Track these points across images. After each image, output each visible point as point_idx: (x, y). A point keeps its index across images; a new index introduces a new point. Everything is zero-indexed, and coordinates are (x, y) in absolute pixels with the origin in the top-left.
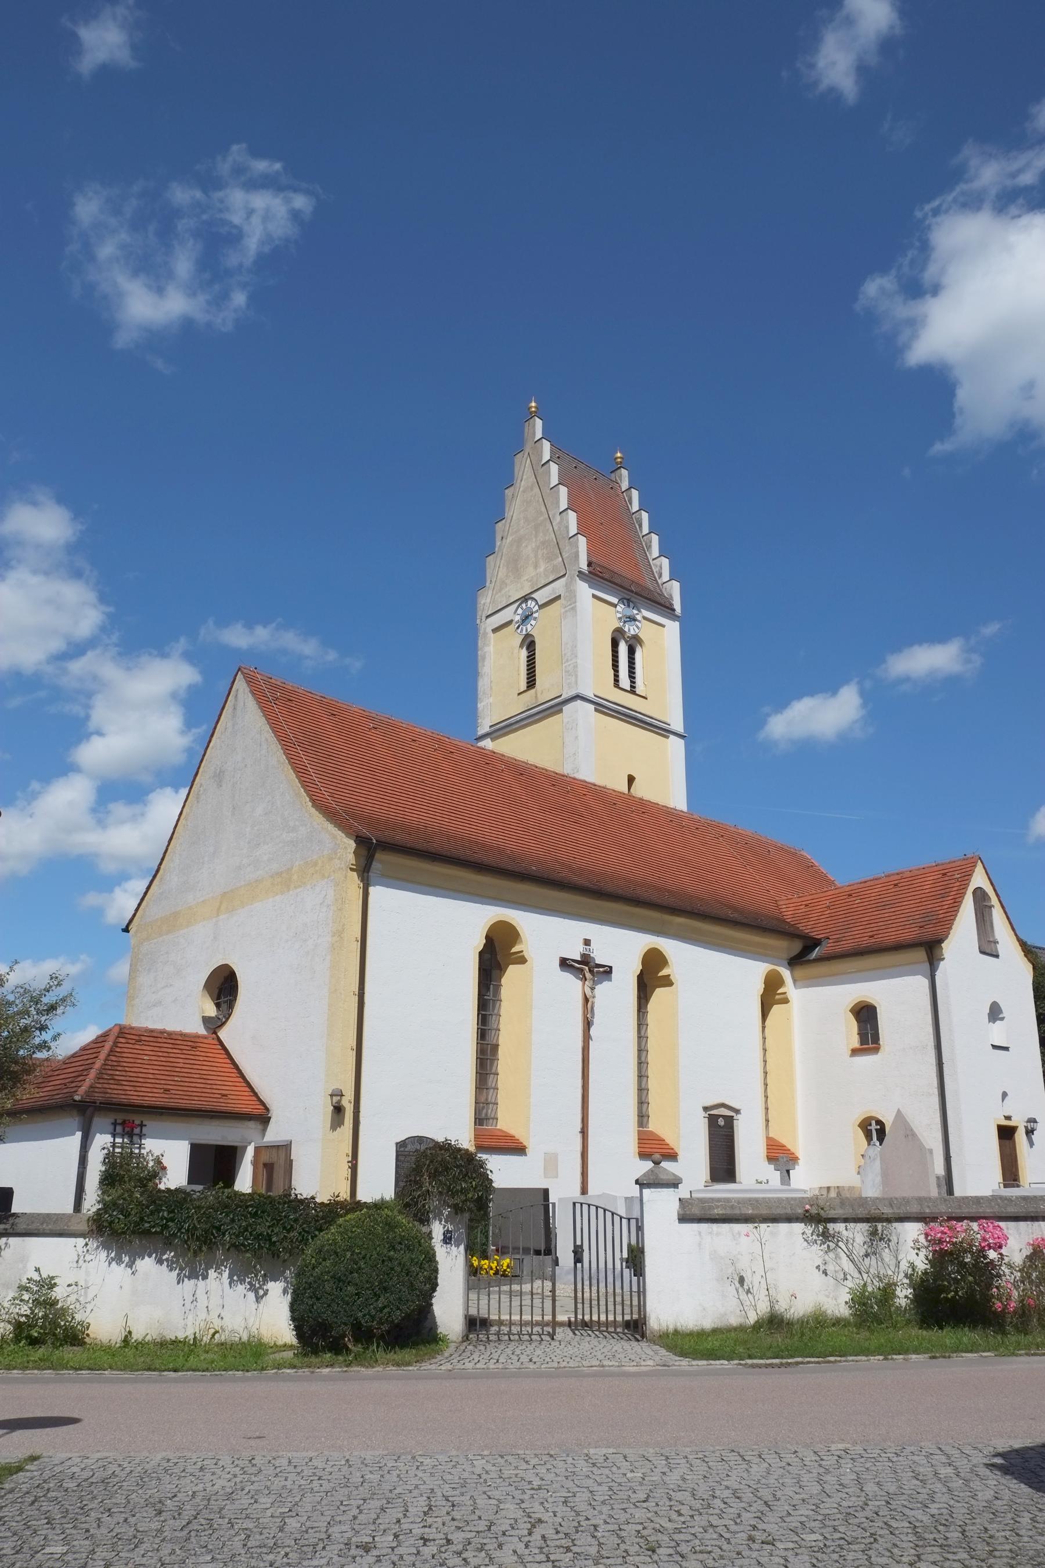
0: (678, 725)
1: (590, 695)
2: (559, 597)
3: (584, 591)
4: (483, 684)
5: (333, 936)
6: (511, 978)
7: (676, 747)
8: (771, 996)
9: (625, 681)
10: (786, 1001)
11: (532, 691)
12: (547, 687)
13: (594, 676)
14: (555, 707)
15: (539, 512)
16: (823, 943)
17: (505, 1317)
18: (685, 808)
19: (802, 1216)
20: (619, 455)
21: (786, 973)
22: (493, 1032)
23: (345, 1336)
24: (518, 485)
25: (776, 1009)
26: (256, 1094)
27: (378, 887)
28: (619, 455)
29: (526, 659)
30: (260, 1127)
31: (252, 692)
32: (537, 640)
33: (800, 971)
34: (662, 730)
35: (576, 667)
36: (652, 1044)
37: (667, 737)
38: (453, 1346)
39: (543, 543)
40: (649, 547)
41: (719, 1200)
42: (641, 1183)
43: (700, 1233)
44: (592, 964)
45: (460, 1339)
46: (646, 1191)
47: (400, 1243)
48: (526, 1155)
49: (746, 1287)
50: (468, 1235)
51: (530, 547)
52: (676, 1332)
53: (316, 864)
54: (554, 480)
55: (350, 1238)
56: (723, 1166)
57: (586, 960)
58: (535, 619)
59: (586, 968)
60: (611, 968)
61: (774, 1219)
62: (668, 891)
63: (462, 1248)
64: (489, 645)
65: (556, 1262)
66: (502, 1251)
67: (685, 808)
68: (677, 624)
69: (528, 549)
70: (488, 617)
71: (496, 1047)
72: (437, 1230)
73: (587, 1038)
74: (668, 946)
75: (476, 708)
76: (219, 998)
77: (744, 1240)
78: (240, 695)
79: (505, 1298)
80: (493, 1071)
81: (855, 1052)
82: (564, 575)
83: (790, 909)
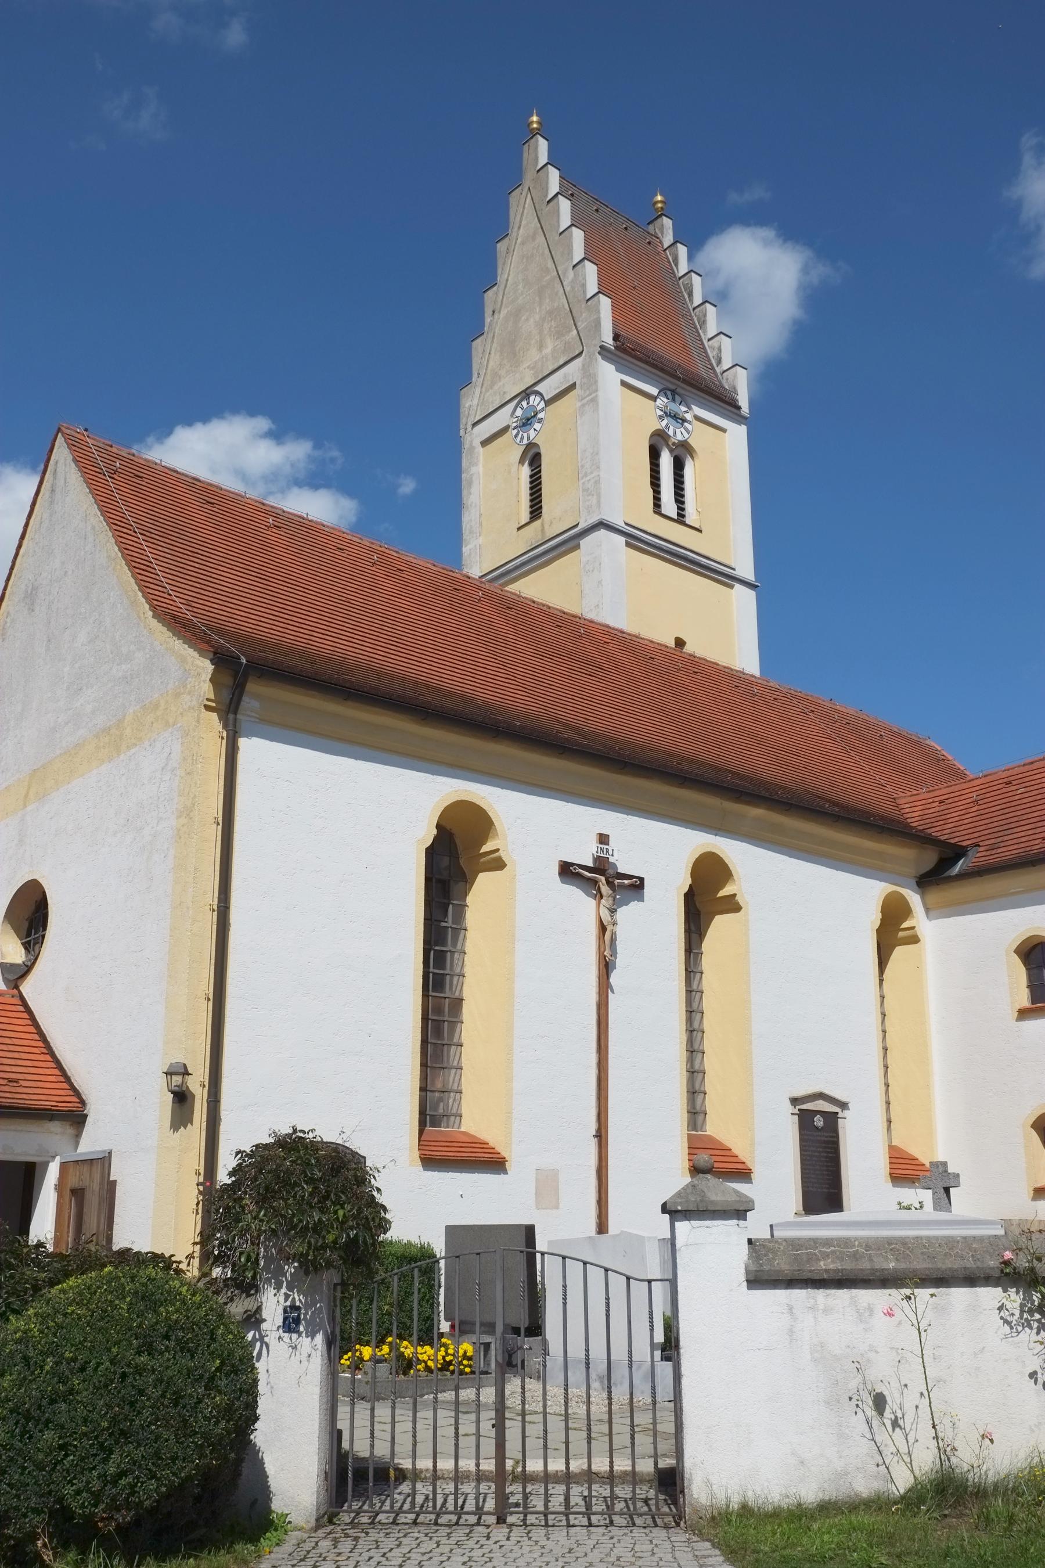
0: (746, 569)
1: (620, 523)
2: (573, 386)
3: (609, 375)
4: (470, 519)
5: (178, 817)
6: (483, 895)
7: (743, 603)
8: (891, 932)
9: (669, 506)
10: (914, 940)
11: (537, 523)
12: (558, 514)
13: (625, 498)
14: (569, 542)
15: (546, 265)
16: (970, 853)
17: (425, 1464)
18: (757, 673)
19: (997, 1274)
20: (659, 198)
21: (914, 899)
22: (455, 979)
23: (33, 1537)
24: (514, 235)
25: (899, 953)
26: (68, 1080)
27: (254, 739)
28: (659, 198)
29: (528, 480)
30: (70, 1131)
31: (75, 460)
32: (543, 451)
33: (936, 895)
34: (726, 578)
35: (597, 482)
36: (709, 1003)
37: (732, 587)
38: (293, 1537)
39: (550, 313)
40: (703, 323)
41: (828, 1242)
42: (673, 1211)
43: (791, 1309)
44: (611, 871)
45: (313, 1523)
46: (681, 1226)
47: (167, 1337)
48: (505, 1172)
49: (888, 1414)
50: (332, 1319)
51: (532, 320)
52: (746, 1510)
53: (157, 706)
54: (565, 220)
55: (60, 1327)
56: (823, 1188)
57: (601, 866)
58: (540, 421)
59: (603, 880)
60: (642, 880)
61: (941, 1280)
62: (732, 773)
63: (319, 1338)
64: (477, 464)
65: (546, 1352)
66: (462, 1329)
67: (757, 673)
68: (744, 428)
69: (529, 325)
70: (475, 424)
71: (457, 1003)
72: (273, 1304)
73: (604, 987)
74: (734, 851)
75: (460, 554)
76: (28, 935)
77: (880, 1321)
78: (61, 468)
79: (445, 1417)
80: (455, 1040)
81: (1023, 1014)
82: (581, 354)
83: (914, 806)
